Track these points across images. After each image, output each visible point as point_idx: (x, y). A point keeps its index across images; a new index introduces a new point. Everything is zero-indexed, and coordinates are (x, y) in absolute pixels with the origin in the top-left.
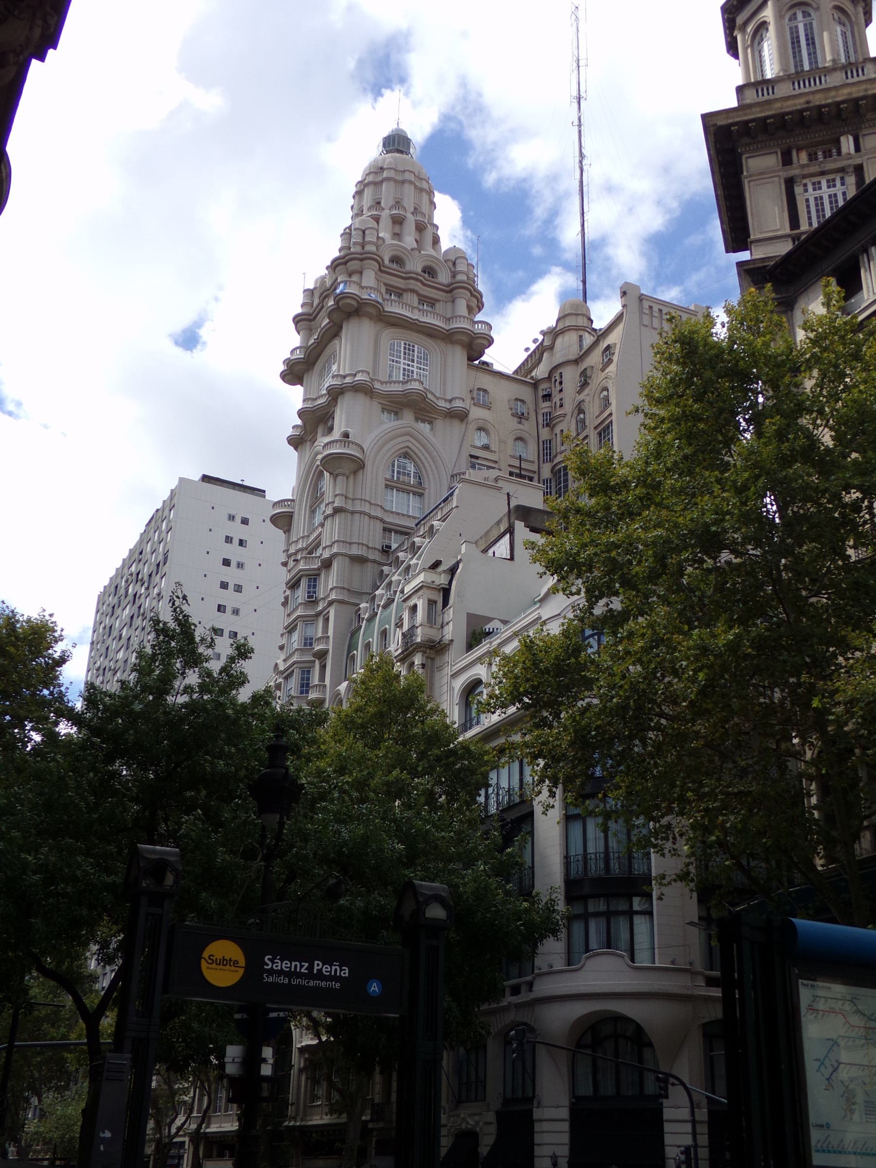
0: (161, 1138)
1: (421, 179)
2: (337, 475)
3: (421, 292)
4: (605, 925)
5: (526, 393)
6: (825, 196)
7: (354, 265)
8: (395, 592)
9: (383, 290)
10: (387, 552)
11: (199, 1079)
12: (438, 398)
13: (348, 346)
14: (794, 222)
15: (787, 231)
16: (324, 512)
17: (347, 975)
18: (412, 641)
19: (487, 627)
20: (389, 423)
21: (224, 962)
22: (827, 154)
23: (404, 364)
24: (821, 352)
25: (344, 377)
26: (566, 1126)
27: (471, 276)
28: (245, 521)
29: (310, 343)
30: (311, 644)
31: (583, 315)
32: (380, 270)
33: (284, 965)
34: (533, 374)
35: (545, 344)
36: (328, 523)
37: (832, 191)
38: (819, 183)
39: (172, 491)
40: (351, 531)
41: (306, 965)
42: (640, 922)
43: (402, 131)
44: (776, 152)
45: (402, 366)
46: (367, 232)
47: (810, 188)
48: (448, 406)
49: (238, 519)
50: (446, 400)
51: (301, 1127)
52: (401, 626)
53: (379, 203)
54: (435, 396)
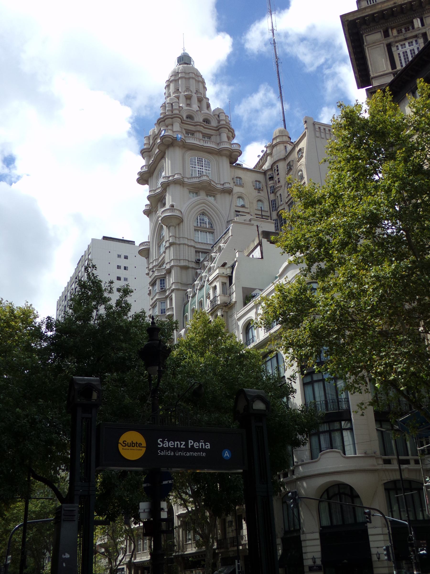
0: (112, 567)
1: (198, 76)
2: (170, 227)
3: (204, 132)
4: (329, 436)
5: (260, 177)
6: (408, 50)
7: (168, 121)
8: (204, 282)
9: (184, 132)
10: (198, 263)
11: (128, 535)
12: (216, 184)
13: (169, 161)
14: (393, 66)
15: (390, 70)
16: (165, 245)
17: (209, 447)
18: (215, 304)
19: (253, 293)
20: (194, 199)
21: (133, 444)
22: (407, 29)
23: (198, 168)
24: (420, 118)
25: (169, 177)
26: (318, 542)
27: (228, 121)
28: (126, 257)
29: (150, 163)
30: (164, 312)
31: (286, 136)
32: (182, 122)
33: (170, 444)
34: (263, 168)
35: (268, 152)
36: (167, 251)
37: (412, 48)
38: (404, 44)
39: (89, 246)
40: (179, 251)
41: (184, 443)
42: (346, 434)
43: (186, 53)
44: (381, 31)
45: (197, 169)
46: (173, 104)
47: (400, 47)
48: (222, 187)
49: (123, 257)
50: (221, 184)
51: (181, 555)
52: (209, 298)
53: (178, 90)
54: (215, 183)
